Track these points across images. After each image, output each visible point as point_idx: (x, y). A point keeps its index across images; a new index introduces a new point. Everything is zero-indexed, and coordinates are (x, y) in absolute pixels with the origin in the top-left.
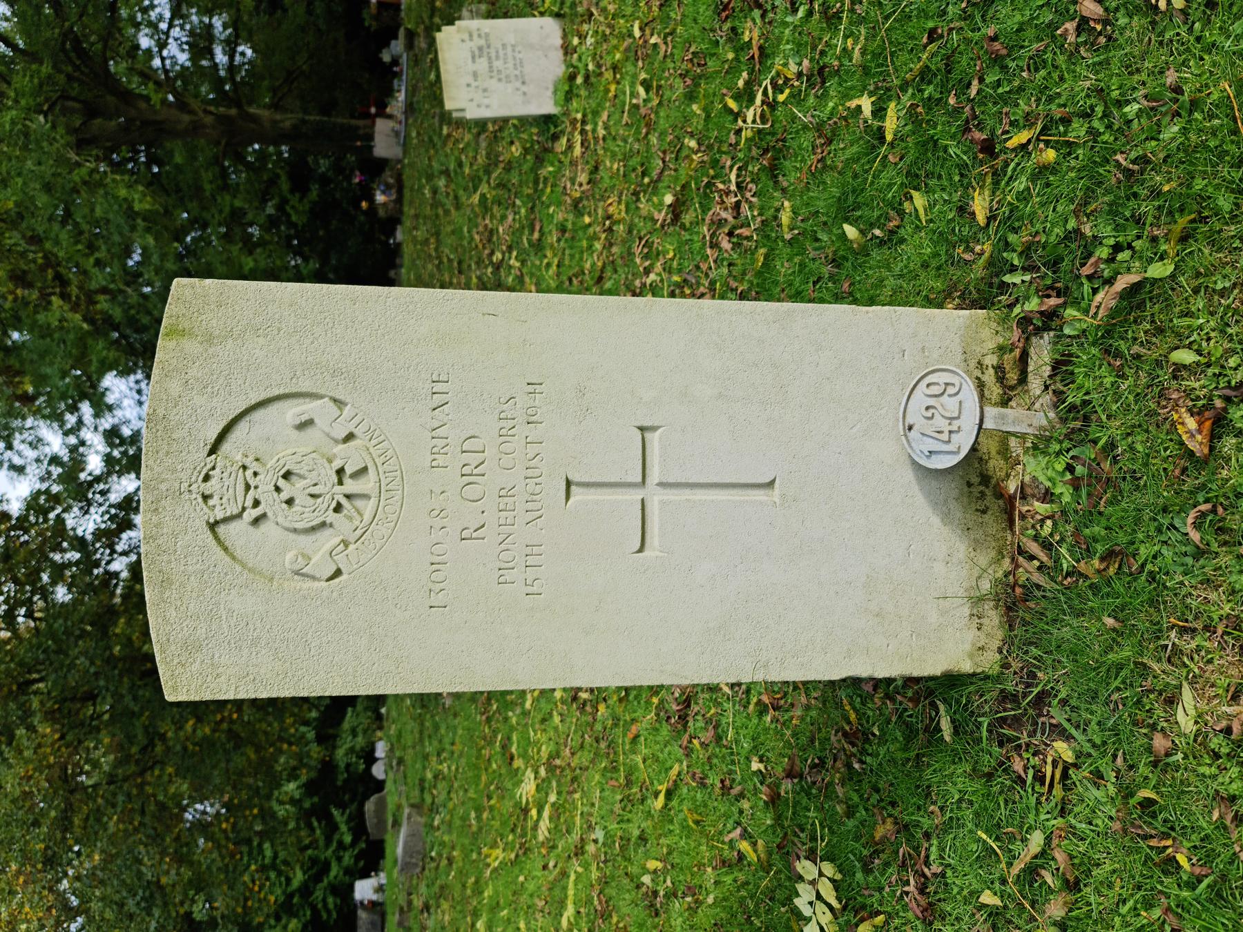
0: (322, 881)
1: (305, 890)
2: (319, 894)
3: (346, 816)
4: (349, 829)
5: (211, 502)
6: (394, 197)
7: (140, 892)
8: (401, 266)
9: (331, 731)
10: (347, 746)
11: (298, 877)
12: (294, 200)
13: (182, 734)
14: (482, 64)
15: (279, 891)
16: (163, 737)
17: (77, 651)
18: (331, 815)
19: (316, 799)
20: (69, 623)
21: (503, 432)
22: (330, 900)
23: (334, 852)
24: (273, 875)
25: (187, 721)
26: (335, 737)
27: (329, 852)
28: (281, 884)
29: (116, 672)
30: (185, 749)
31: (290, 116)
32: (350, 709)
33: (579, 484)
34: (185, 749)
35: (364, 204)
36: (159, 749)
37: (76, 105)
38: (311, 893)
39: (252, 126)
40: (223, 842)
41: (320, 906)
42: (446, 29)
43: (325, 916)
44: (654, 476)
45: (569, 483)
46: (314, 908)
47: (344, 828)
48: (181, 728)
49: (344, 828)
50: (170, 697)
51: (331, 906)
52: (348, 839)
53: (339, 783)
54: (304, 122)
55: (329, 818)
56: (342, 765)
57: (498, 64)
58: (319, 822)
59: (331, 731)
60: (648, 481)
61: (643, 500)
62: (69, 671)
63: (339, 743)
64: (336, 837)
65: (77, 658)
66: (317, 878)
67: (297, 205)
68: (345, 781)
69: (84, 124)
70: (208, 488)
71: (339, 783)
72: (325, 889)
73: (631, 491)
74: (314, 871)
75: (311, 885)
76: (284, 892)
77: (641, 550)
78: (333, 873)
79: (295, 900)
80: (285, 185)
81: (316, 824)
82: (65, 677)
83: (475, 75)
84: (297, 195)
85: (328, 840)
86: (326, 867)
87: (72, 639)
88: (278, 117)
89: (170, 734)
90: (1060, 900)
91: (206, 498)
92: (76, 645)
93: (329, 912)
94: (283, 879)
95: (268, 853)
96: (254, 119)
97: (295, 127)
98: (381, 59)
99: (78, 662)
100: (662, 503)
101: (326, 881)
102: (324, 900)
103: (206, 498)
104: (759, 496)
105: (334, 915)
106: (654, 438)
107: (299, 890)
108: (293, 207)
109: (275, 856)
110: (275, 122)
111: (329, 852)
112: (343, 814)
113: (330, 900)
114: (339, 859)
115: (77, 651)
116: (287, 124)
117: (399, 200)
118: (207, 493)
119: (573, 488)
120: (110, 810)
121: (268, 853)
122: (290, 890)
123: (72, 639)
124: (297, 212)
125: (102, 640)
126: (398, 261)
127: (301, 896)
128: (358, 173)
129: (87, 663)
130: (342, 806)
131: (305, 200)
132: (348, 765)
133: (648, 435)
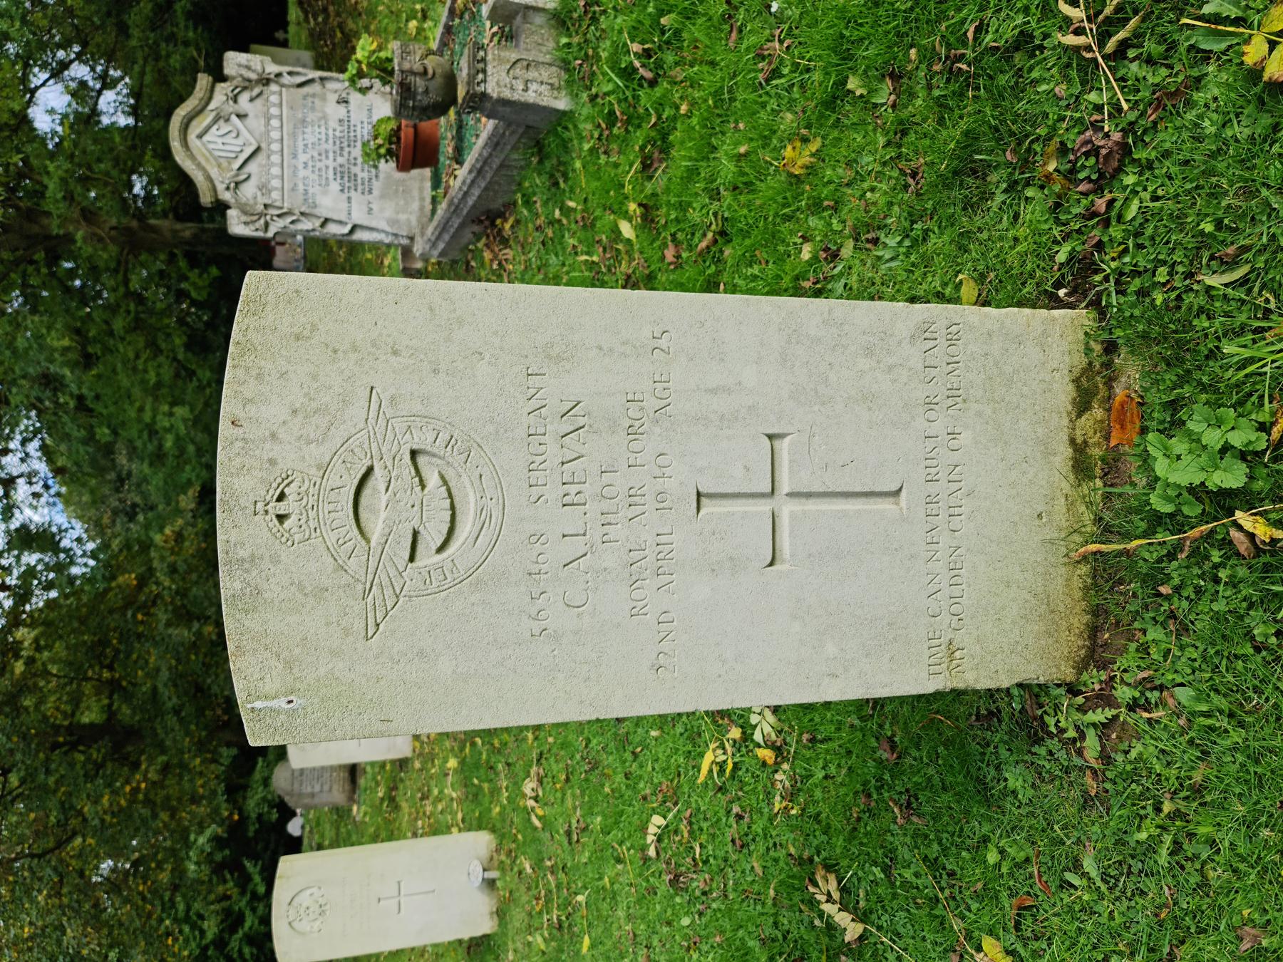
0: (237, 932)
2: (234, 943)
3: (259, 867)
4: (263, 880)
5: (287, 524)
9: (241, 781)
10: (259, 796)
15: (193, 945)
18: (244, 867)
19: (227, 852)
22: (247, 950)
23: (248, 903)
24: (186, 929)
26: (245, 787)
28: (195, 938)
32: (260, 760)
33: (711, 496)
38: (227, 944)
39: (154, 236)
40: (140, 903)
44: (785, 486)
45: (699, 495)
50: (252, 743)
53: (251, 834)
54: (203, 230)
55: (242, 869)
56: (253, 816)
58: (232, 875)
59: (241, 781)
60: (776, 493)
63: (249, 794)
64: (250, 887)
66: (233, 929)
68: (256, 832)
70: (282, 508)
71: (251, 834)
72: (241, 940)
73: (763, 501)
74: (229, 922)
76: (199, 946)
77: (771, 564)
78: (248, 924)
79: (210, 953)
81: (228, 876)
84: (196, 271)
86: (240, 919)
88: (178, 226)
91: (281, 518)
94: (197, 933)
95: (181, 907)
96: (153, 229)
97: (195, 236)
100: (793, 516)
101: (241, 932)
102: (240, 951)
103: (281, 518)
104: (885, 505)
106: (784, 446)
107: (213, 942)
109: (188, 909)
110: (175, 232)
111: (243, 903)
112: (255, 865)
113: (247, 950)
114: (254, 910)
116: (187, 234)
118: (281, 512)
119: (703, 500)
121: (181, 907)
122: (204, 942)
127: (216, 948)
130: (255, 857)
131: (205, 276)
132: (260, 816)
133: (777, 443)
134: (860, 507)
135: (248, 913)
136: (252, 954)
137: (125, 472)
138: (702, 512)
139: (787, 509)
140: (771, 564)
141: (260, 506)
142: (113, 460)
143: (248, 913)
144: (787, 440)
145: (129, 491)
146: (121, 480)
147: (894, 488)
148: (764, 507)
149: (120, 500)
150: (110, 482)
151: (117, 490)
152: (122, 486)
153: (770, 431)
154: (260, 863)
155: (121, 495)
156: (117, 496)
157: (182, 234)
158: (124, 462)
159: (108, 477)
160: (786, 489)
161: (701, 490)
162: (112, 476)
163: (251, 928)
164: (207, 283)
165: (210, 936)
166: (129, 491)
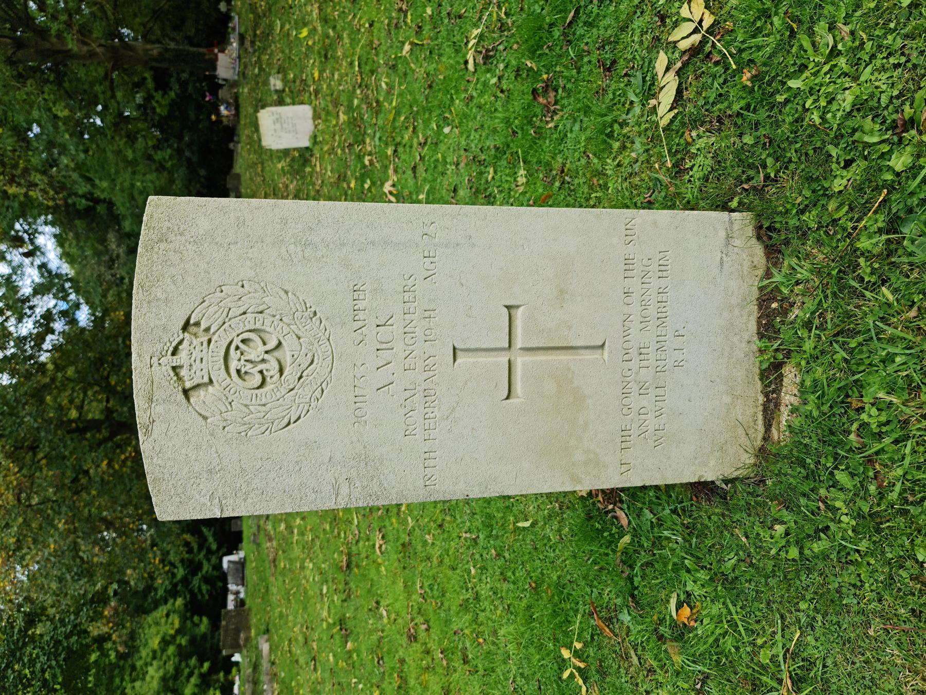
1: (185, 581)
3: (212, 532)
4: (215, 540)
6: (233, 112)
7: (75, 570)
8: (239, 142)
11: (180, 572)
12: (158, 96)
13: (100, 469)
14: (278, 126)
16: (86, 472)
17: (24, 412)
20: (18, 394)
21: (658, 369)
25: (102, 461)
27: (201, 556)
29: (52, 426)
30: (102, 480)
31: (157, 46)
33: (462, 350)
34: (102, 480)
35: (213, 117)
36: (84, 481)
37: (8, 41)
39: (131, 53)
41: (196, 591)
42: (262, 111)
43: (199, 597)
44: (519, 343)
45: (454, 349)
46: (192, 593)
47: (211, 539)
48: (98, 466)
49: (211, 539)
51: (204, 592)
52: (214, 547)
54: (167, 50)
57: (284, 126)
60: (513, 348)
61: (509, 361)
62: (20, 426)
64: (207, 545)
65: (25, 417)
67: (160, 100)
69: (14, 53)
75: (189, 577)
76: (171, 583)
77: (508, 398)
79: (179, 588)
80: (150, 84)
82: (17, 430)
83: (275, 130)
84: (160, 92)
85: (200, 548)
86: (200, 566)
87: (20, 406)
89: (91, 471)
90: (50, 86)
92: (24, 409)
93: (203, 595)
97: (160, 54)
98: (219, 9)
99: (26, 420)
100: (524, 364)
101: (200, 574)
102: (199, 587)
105: (207, 597)
108: (157, 102)
110: (147, 50)
111: (201, 556)
112: (210, 530)
114: (209, 560)
115: (24, 412)
116: (155, 52)
117: (237, 114)
119: (459, 353)
120: (57, 517)
122: (175, 581)
123: (20, 406)
124: (160, 105)
125: (41, 405)
126: (235, 139)
128: (208, 94)
129: (32, 420)
131: (166, 96)
134: (571, 357)
135: (205, 562)
136: (208, 591)
137: (115, 255)
138: (458, 361)
139: (520, 361)
140: (508, 398)
141: (155, 359)
142: (106, 247)
143: (205, 562)
144: (521, 309)
145: (118, 268)
146: (112, 261)
147: (600, 344)
148: (503, 359)
149: (113, 275)
150: (105, 262)
151: (110, 268)
152: (113, 264)
153: (508, 303)
154: (213, 529)
155: (113, 271)
156: (109, 272)
157: (151, 52)
158: (114, 247)
159: (104, 259)
160: (519, 345)
161: (457, 346)
162: (106, 258)
163: (207, 572)
164: (167, 102)
165: (179, 576)
166: (118, 268)
